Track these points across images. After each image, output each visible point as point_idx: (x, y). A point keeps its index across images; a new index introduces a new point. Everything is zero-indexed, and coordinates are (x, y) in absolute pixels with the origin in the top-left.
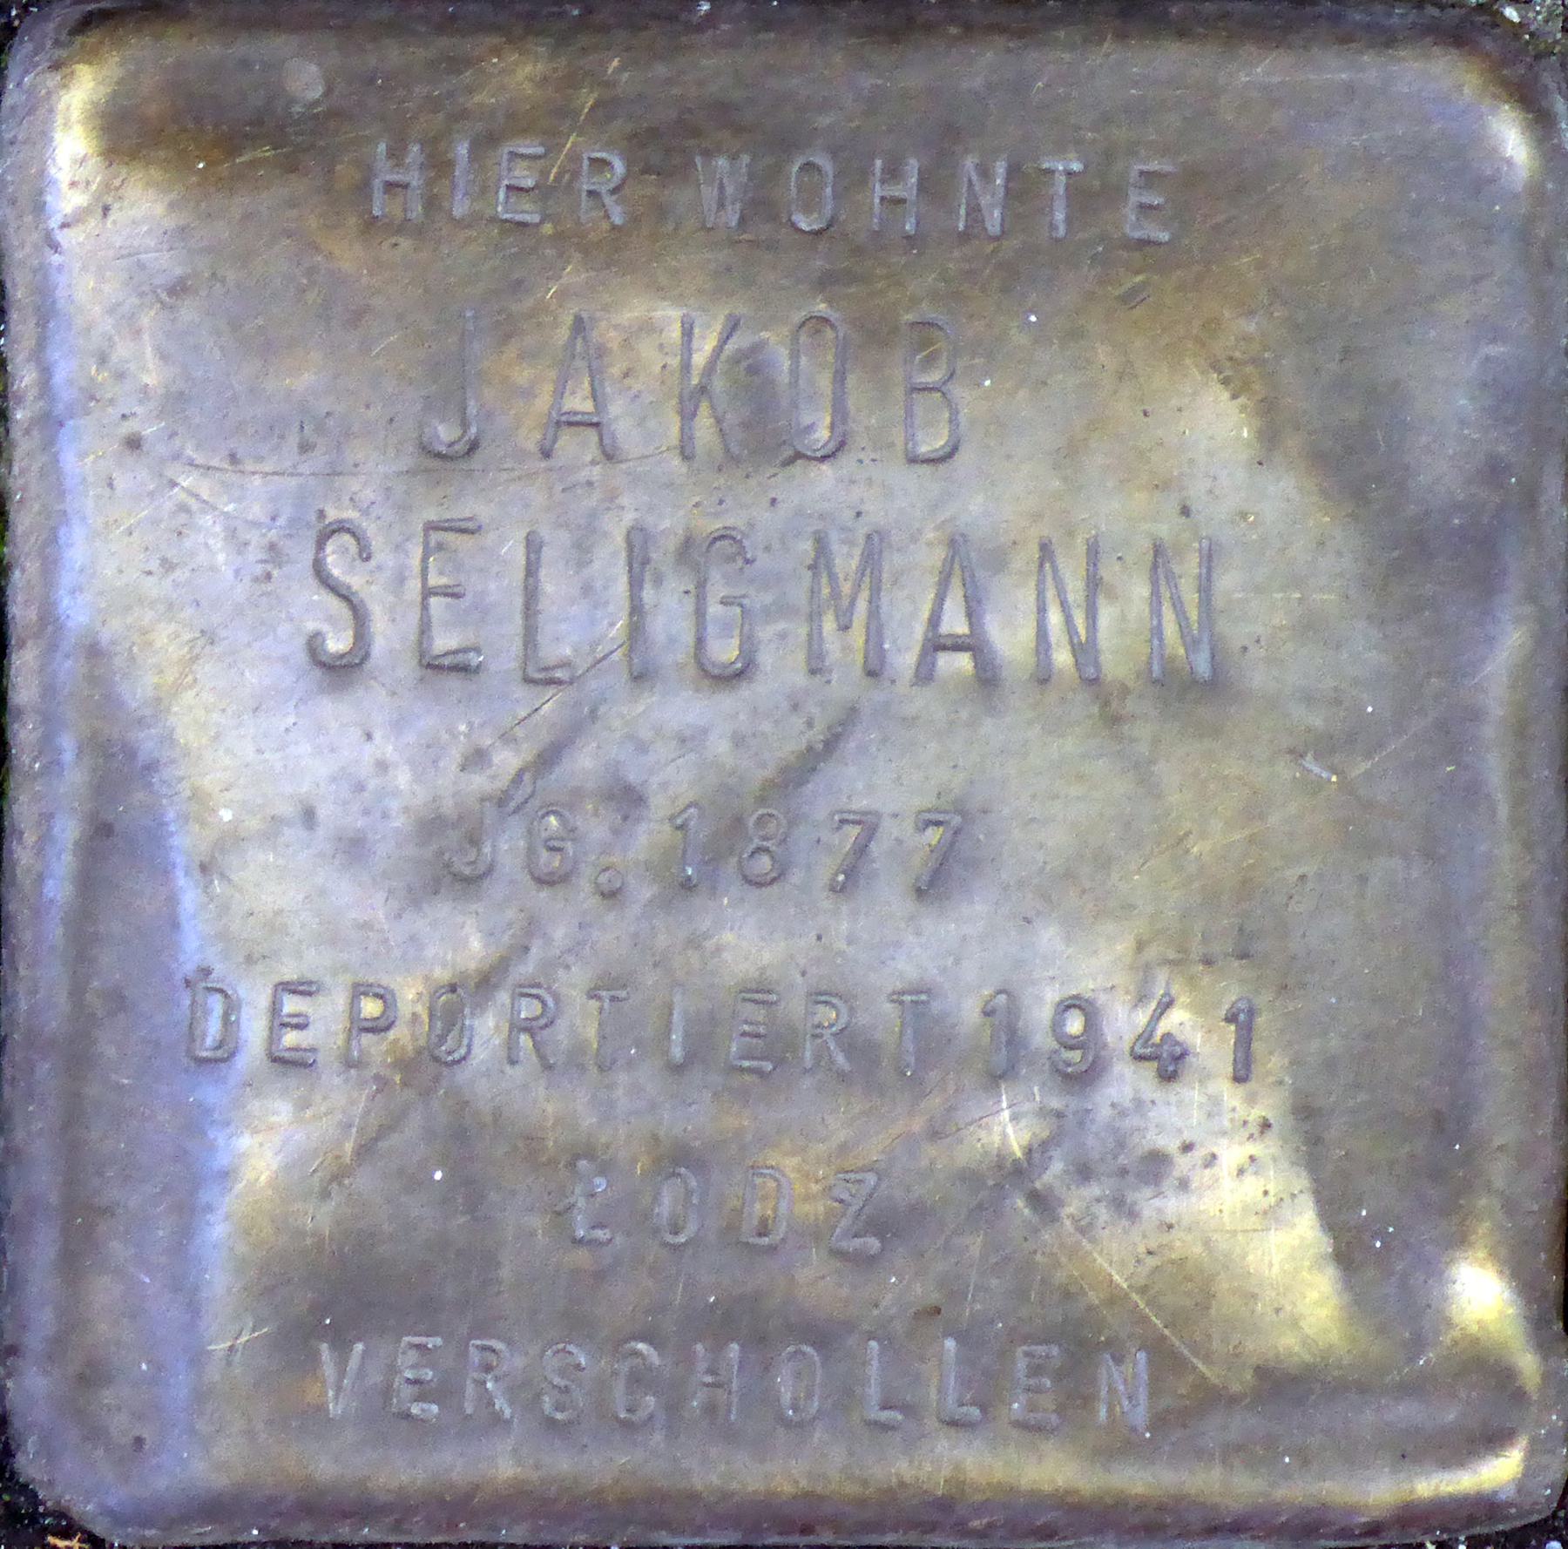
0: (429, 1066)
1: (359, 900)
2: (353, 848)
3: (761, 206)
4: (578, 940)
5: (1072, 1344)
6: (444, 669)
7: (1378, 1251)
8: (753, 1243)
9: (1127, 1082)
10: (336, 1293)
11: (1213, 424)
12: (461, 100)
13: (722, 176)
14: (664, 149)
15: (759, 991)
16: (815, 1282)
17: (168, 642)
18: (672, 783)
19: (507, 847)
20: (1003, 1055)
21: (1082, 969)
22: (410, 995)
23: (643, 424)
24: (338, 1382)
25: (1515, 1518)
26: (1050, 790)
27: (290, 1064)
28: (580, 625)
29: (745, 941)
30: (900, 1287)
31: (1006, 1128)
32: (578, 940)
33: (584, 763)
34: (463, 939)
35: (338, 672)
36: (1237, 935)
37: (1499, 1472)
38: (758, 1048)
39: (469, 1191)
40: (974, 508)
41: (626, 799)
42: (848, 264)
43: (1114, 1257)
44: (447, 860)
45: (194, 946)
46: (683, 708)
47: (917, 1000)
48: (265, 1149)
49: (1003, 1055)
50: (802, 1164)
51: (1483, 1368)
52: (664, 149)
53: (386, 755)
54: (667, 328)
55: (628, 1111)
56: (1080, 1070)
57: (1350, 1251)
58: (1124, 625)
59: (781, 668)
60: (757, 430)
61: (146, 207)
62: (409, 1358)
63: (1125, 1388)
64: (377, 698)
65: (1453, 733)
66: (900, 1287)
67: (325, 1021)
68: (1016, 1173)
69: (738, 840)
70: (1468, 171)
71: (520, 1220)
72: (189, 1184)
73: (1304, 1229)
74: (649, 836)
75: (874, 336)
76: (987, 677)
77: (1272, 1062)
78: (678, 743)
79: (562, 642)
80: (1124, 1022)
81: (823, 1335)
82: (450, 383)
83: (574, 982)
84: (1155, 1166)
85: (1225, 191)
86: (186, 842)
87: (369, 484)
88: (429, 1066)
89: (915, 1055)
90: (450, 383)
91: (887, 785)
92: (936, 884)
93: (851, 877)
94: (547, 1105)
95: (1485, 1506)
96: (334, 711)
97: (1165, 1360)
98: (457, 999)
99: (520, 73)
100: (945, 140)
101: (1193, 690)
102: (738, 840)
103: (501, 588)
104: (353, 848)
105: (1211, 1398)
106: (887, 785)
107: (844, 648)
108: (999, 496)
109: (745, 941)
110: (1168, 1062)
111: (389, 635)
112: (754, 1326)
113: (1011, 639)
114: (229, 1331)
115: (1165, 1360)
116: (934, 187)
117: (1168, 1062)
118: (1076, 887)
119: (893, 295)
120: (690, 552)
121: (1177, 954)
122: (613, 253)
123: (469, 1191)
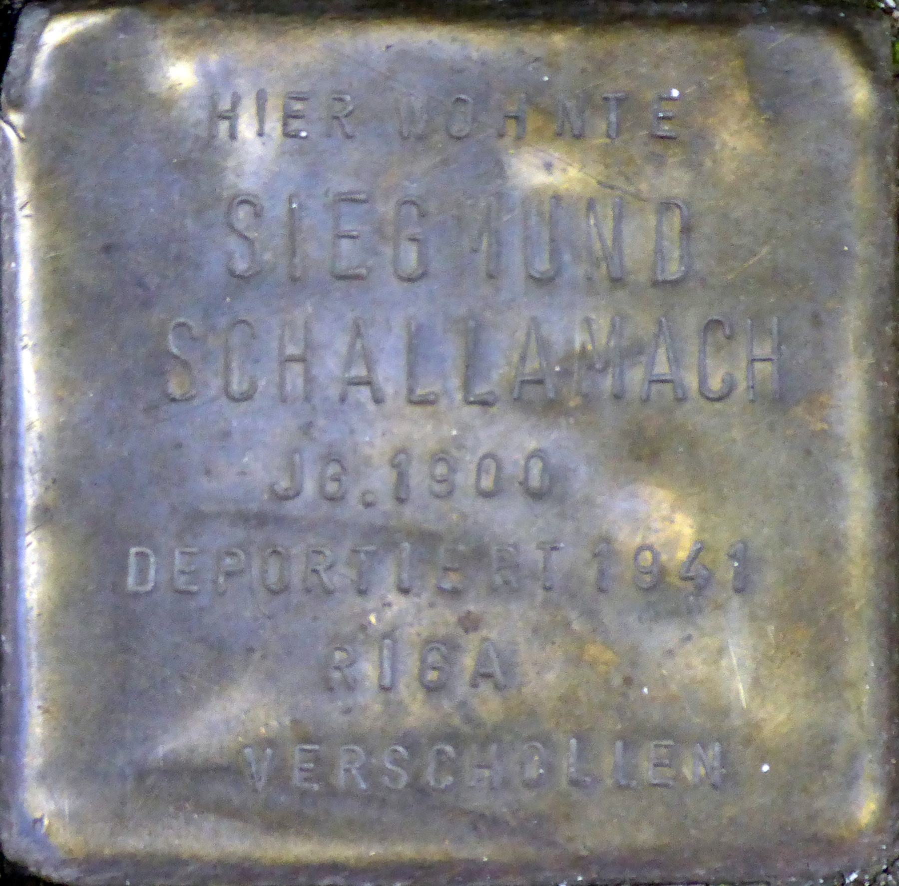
25: (486, 824)
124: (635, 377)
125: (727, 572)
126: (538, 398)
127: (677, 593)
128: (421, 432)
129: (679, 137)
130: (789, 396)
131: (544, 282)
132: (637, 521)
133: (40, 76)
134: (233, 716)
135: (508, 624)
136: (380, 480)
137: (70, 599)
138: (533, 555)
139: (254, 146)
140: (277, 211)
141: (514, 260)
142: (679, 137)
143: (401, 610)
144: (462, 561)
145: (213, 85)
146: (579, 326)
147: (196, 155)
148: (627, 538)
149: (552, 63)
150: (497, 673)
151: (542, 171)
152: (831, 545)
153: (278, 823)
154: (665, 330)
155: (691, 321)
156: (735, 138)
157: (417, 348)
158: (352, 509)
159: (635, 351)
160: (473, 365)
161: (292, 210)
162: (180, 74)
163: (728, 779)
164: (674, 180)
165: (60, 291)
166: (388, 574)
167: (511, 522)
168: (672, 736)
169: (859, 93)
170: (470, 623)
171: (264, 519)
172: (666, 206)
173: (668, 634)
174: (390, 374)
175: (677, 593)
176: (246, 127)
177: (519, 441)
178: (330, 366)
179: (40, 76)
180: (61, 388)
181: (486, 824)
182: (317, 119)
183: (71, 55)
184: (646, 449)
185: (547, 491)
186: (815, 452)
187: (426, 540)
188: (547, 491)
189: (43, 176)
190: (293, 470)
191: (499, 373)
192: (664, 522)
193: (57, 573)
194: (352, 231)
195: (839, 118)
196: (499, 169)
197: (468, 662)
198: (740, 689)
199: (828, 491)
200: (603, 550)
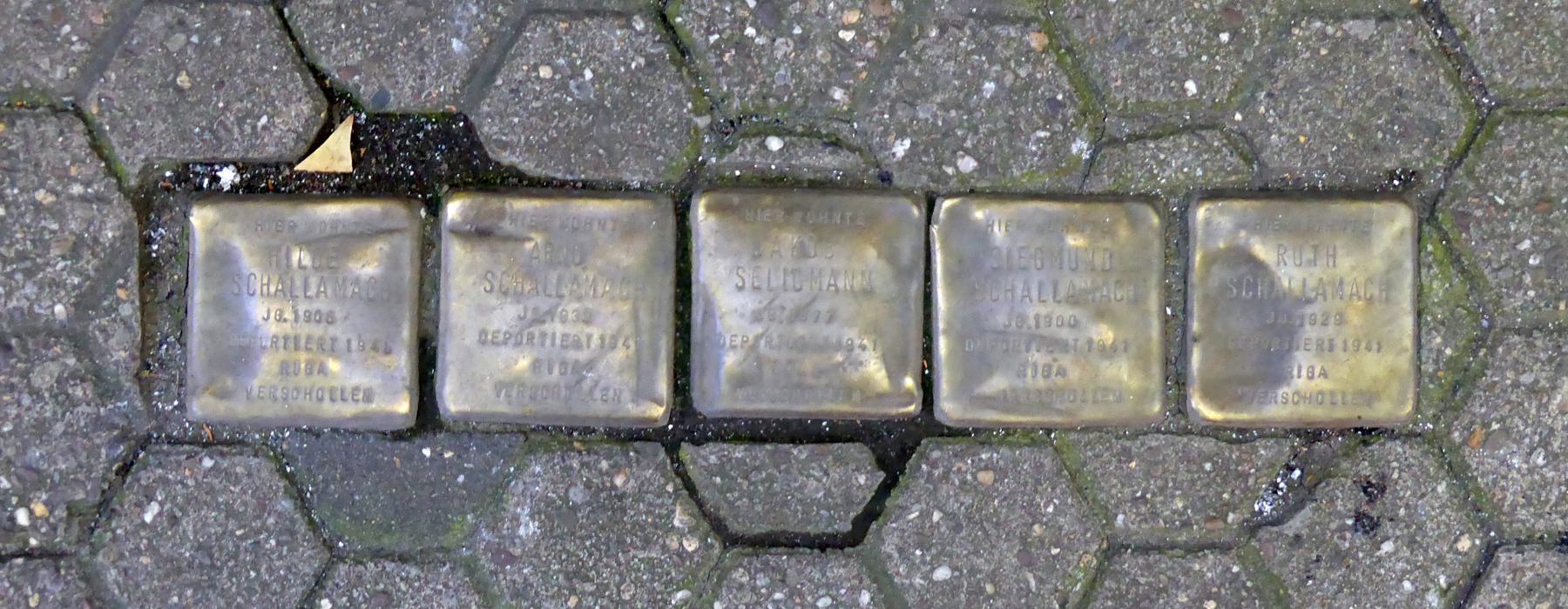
0: (754, 347)
1: (744, 323)
2: (742, 315)
3: (804, 220)
4: (775, 331)
5: (848, 390)
6: (756, 289)
7: (894, 375)
8: (802, 374)
9: (857, 351)
10: (741, 381)
11: (871, 253)
12: (78, 213)
13: (798, 215)
14: (789, 211)
15: (803, 337)
16: (811, 381)
17: (715, 284)
18: (790, 306)
19: (765, 316)
20: (838, 347)
21: (851, 334)
22: (751, 337)
23: (787, 253)
24: (741, 393)
25: (1060, 412)
26: (847, 308)
27: (733, 347)
28: (776, 282)
29: (800, 330)
30: (823, 381)
31: (839, 358)
32: (775, 331)
33: (777, 302)
34: (759, 329)
35: (740, 289)
36: (874, 330)
37: (912, 408)
38: (802, 346)
39: (760, 366)
40: (835, 265)
41: (783, 308)
42: (816, 228)
43: (854, 376)
44: (757, 317)
45: (719, 328)
46: (793, 295)
47: (826, 339)
48: (730, 360)
49: (838, 347)
50: (809, 363)
51: (909, 393)
52: (789, 211)
53: (748, 302)
54: (790, 238)
55: (782, 355)
56: (850, 349)
57: (890, 375)
58: (858, 282)
59: (806, 287)
60: (802, 253)
61: (712, 219)
62: (750, 390)
63: (856, 396)
64: (745, 293)
65: (906, 300)
66: (823, 381)
67: (738, 341)
68: (840, 364)
69: (799, 314)
70: (908, 214)
71: (767, 370)
72: (719, 364)
73: (883, 373)
74: (786, 313)
75: (820, 240)
76: (837, 290)
77: (879, 348)
78: (790, 300)
79: (774, 284)
80: (857, 342)
81: (811, 388)
82: (757, 246)
83: (775, 336)
84: (861, 363)
85: (873, 219)
86: (718, 314)
87: (744, 261)
88: (754, 347)
89: (824, 347)
90: (757, 246)
91: (823, 306)
92: (830, 320)
93: (817, 320)
94: (773, 354)
95: (908, 414)
96: (740, 295)
97: (862, 392)
98: (758, 338)
99: (768, 200)
100: (831, 210)
101: (868, 293)
102: (799, 314)
103: (764, 275)
104: (742, 315)
105: (868, 398)
106: (823, 306)
107: (815, 286)
108: (839, 263)
109: (800, 330)
110: (864, 348)
111: (496, 287)
112: (800, 386)
113: (841, 284)
114: (725, 387)
115: (862, 392)
116: (830, 217)
117: (864, 348)
118: (850, 323)
119: (823, 233)
120: (793, 271)
121: (864, 332)
122: (780, 227)
123: (760, 366)
124: (1098, 295)
125: (1121, 347)
126: (1074, 300)
127: (1108, 352)
128: (1043, 310)
129: (1109, 232)
130: (1138, 301)
131: (1074, 270)
132: (1099, 334)
133: (942, 215)
134: (997, 384)
135: (1066, 360)
136: (1032, 322)
137: (952, 353)
138: (1071, 342)
139: (999, 233)
140: (1005, 252)
141: (1066, 264)
142: (1109, 232)
143: (1038, 357)
144: (1054, 345)
145: (988, 218)
146: (1082, 282)
147: (982, 234)
148: (1096, 338)
149: (1075, 212)
150: (1062, 372)
151: (1074, 241)
152: (1149, 339)
153: (1007, 411)
154: (1105, 284)
155: (1112, 281)
156: (1123, 232)
157: (1041, 286)
158: (1025, 329)
159: (1097, 289)
160: (1055, 293)
161: (150, 436)
162: (979, 215)
163: (1119, 400)
164: (1107, 243)
165: (948, 271)
166: (1034, 347)
167: (1065, 334)
168: (1106, 390)
169: (1155, 220)
170: (1055, 360)
171: (1002, 333)
172: (1105, 250)
173: (1106, 363)
174: (1034, 294)
175: (1108, 352)
176: (996, 228)
177: (1068, 312)
178: (1019, 292)
179: (942, 215)
180: (948, 298)
181: (1060, 412)
182: (1017, 226)
183: (951, 211)
184: (1101, 314)
185: (1075, 325)
186: (1145, 314)
187: (1042, 338)
188: (1075, 325)
189: (943, 242)
190: (1010, 320)
191: (1062, 292)
192: (1105, 334)
193: (948, 345)
194: (505, 146)
195: (1150, 227)
196: (1062, 239)
197: (1055, 370)
198: (1125, 377)
199: (1148, 325)
200: (1090, 342)
